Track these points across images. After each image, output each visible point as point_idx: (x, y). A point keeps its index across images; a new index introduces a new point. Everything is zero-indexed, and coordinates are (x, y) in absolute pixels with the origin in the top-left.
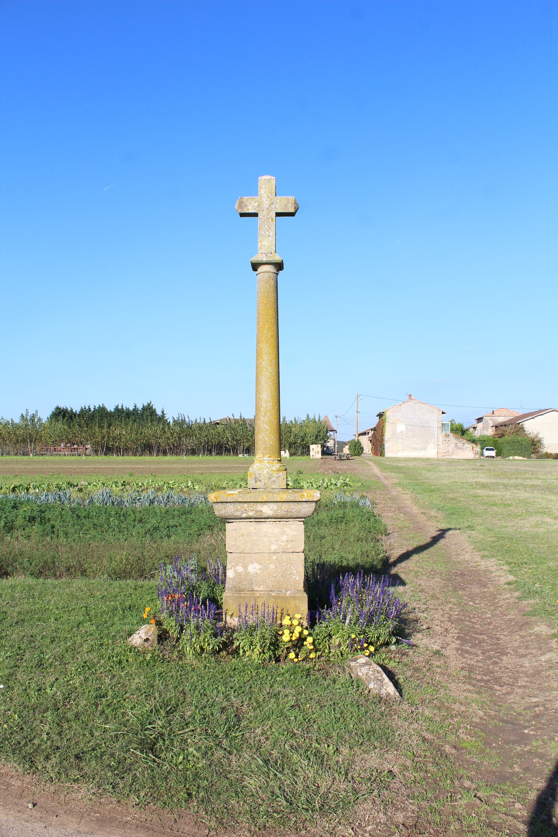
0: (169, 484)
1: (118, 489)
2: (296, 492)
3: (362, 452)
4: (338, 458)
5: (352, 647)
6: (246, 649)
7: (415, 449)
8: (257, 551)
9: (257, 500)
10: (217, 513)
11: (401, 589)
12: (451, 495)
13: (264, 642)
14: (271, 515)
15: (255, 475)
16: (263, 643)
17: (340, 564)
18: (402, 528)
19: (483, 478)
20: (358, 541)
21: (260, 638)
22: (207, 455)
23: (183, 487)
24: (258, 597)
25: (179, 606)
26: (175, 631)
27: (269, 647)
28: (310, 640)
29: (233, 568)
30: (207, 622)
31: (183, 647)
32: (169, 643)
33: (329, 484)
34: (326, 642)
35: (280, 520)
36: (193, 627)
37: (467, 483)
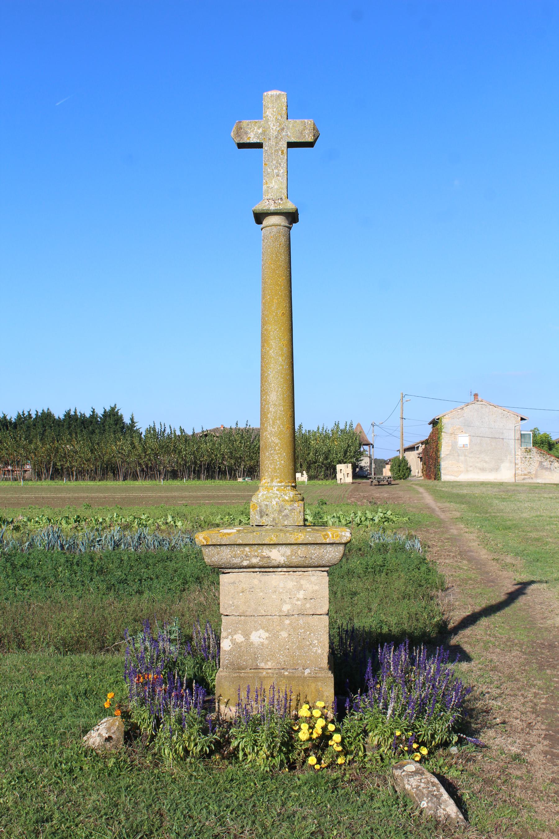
0: (141, 519)
1: (70, 526)
2: (317, 530)
4: (375, 482)
5: (396, 748)
6: (247, 751)
7: (483, 470)
8: (264, 613)
9: (264, 542)
10: (207, 560)
11: (464, 666)
12: (534, 535)
13: (273, 741)
14: (282, 562)
15: (260, 506)
16: (271, 743)
17: (379, 631)
18: (465, 581)
21: (267, 736)
22: (193, 479)
23: (160, 523)
24: (264, 677)
25: (154, 691)
26: (148, 726)
27: (280, 748)
28: (337, 738)
29: (230, 637)
30: (194, 712)
31: (160, 749)
32: (140, 744)
33: (363, 519)
34: (359, 741)
35: (295, 569)
36: (173, 720)
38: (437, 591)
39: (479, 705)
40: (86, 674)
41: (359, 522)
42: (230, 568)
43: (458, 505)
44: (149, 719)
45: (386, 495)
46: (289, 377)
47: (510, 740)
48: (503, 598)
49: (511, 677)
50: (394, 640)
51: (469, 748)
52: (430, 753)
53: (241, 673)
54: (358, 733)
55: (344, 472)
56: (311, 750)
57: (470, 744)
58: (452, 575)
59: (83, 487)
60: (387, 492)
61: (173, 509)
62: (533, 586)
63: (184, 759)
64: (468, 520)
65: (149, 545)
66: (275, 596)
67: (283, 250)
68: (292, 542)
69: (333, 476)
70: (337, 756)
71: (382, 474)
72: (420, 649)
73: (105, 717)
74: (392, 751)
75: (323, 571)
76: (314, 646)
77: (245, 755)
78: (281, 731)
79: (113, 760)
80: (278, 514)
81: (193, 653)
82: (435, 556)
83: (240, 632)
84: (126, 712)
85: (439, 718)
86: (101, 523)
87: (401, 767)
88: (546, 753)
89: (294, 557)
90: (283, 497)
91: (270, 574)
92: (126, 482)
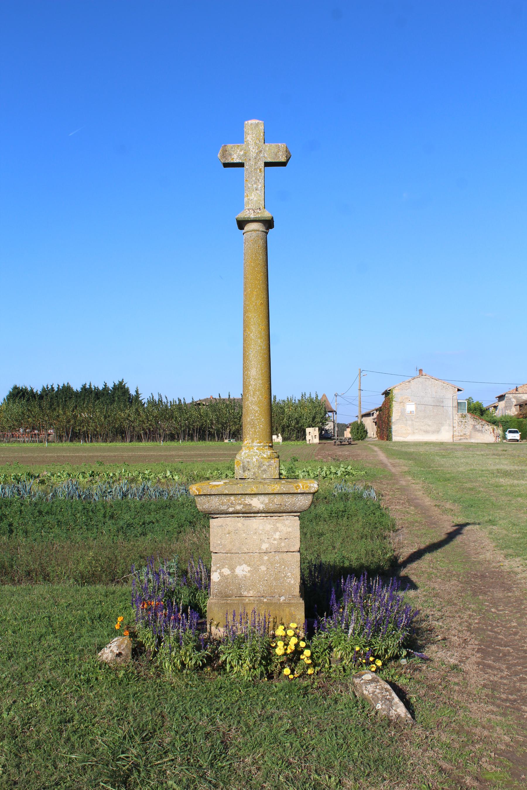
0: (144, 474)
1: (86, 480)
2: (290, 482)
3: (366, 436)
4: (338, 442)
5: (356, 661)
6: (233, 664)
7: (427, 432)
8: (246, 551)
9: (246, 492)
10: (199, 507)
11: (412, 593)
12: (468, 485)
13: (255, 655)
14: (261, 508)
15: (243, 463)
16: (253, 658)
18: (412, 523)
19: (505, 465)
20: (362, 538)
22: (188, 441)
23: (161, 477)
24: (247, 604)
25: (156, 615)
26: (152, 644)
27: (260, 661)
28: (307, 653)
31: (161, 663)
32: (145, 658)
33: (328, 473)
34: (326, 655)
35: (272, 515)
36: (172, 639)
37: (487, 470)
39: (424, 625)
41: (325, 475)
42: (218, 514)
43: (406, 461)
44: (153, 638)
45: (347, 453)
46: (266, 356)
47: (449, 653)
48: (443, 537)
49: (450, 602)
51: (416, 661)
52: (383, 664)
55: (312, 434)
56: (286, 663)
60: (348, 451)
62: (468, 528)
63: (181, 671)
64: (414, 473)
67: (261, 251)
69: (304, 437)
70: (308, 668)
71: (344, 436)
76: (288, 578)
77: (232, 667)
78: (261, 648)
79: (123, 672)
81: (189, 585)
82: (388, 503)
83: (227, 566)
86: (112, 477)
87: (360, 676)
88: (478, 664)
89: (271, 505)
92: (132, 443)
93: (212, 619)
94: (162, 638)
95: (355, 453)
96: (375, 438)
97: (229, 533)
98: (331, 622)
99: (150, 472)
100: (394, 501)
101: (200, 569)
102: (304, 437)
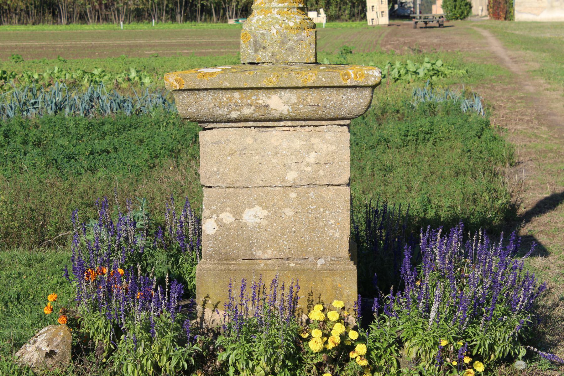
0: (93, 75)
2: (334, 68)
3: (469, 12)
4: (421, 23)
5: (441, 363)
6: (240, 366)
9: (259, 85)
11: (538, 261)
13: (274, 353)
14: (285, 113)
15: (254, 36)
16: (271, 356)
17: (422, 215)
18: (543, 153)
20: (457, 174)
21: (266, 346)
22: (166, 21)
23: (120, 80)
25: (110, 291)
26: (105, 337)
27: (284, 362)
28: (361, 349)
29: (214, 216)
30: (166, 317)
31: (121, 364)
32: (94, 360)
33: (403, 71)
34: (391, 353)
35: (303, 123)
36: (138, 327)
38: (504, 166)
40: (19, 273)
41: (397, 76)
42: (213, 122)
43: (537, 54)
44: (106, 328)
45: (435, 41)
50: (447, 226)
52: (486, 371)
53: (230, 265)
54: (389, 344)
56: (325, 365)
57: (543, 361)
58: (525, 146)
59: (9, 34)
60: (438, 37)
61: (138, 61)
64: (550, 73)
65: (105, 108)
66: (276, 161)
68: (300, 85)
69: (362, 15)
71: (431, 13)
72: (478, 234)
73: (45, 326)
74: (436, 366)
75: (341, 125)
76: (330, 228)
78: (285, 340)
80: (280, 47)
81: (167, 246)
82: (503, 120)
83: (228, 209)
84: (75, 319)
85: (501, 323)
86: (37, 81)
90: (286, 24)
91: (269, 129)
92: (71, 26)
93: (207, 296)
94: (122, 324)
95: (450, 41)
96: (486, 16)
97: (232, 155)
98: (401, 300)
99: (103, 71)
100: (514, 116)
101: (186, 217)
102: (362, 15)
